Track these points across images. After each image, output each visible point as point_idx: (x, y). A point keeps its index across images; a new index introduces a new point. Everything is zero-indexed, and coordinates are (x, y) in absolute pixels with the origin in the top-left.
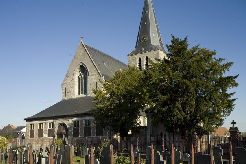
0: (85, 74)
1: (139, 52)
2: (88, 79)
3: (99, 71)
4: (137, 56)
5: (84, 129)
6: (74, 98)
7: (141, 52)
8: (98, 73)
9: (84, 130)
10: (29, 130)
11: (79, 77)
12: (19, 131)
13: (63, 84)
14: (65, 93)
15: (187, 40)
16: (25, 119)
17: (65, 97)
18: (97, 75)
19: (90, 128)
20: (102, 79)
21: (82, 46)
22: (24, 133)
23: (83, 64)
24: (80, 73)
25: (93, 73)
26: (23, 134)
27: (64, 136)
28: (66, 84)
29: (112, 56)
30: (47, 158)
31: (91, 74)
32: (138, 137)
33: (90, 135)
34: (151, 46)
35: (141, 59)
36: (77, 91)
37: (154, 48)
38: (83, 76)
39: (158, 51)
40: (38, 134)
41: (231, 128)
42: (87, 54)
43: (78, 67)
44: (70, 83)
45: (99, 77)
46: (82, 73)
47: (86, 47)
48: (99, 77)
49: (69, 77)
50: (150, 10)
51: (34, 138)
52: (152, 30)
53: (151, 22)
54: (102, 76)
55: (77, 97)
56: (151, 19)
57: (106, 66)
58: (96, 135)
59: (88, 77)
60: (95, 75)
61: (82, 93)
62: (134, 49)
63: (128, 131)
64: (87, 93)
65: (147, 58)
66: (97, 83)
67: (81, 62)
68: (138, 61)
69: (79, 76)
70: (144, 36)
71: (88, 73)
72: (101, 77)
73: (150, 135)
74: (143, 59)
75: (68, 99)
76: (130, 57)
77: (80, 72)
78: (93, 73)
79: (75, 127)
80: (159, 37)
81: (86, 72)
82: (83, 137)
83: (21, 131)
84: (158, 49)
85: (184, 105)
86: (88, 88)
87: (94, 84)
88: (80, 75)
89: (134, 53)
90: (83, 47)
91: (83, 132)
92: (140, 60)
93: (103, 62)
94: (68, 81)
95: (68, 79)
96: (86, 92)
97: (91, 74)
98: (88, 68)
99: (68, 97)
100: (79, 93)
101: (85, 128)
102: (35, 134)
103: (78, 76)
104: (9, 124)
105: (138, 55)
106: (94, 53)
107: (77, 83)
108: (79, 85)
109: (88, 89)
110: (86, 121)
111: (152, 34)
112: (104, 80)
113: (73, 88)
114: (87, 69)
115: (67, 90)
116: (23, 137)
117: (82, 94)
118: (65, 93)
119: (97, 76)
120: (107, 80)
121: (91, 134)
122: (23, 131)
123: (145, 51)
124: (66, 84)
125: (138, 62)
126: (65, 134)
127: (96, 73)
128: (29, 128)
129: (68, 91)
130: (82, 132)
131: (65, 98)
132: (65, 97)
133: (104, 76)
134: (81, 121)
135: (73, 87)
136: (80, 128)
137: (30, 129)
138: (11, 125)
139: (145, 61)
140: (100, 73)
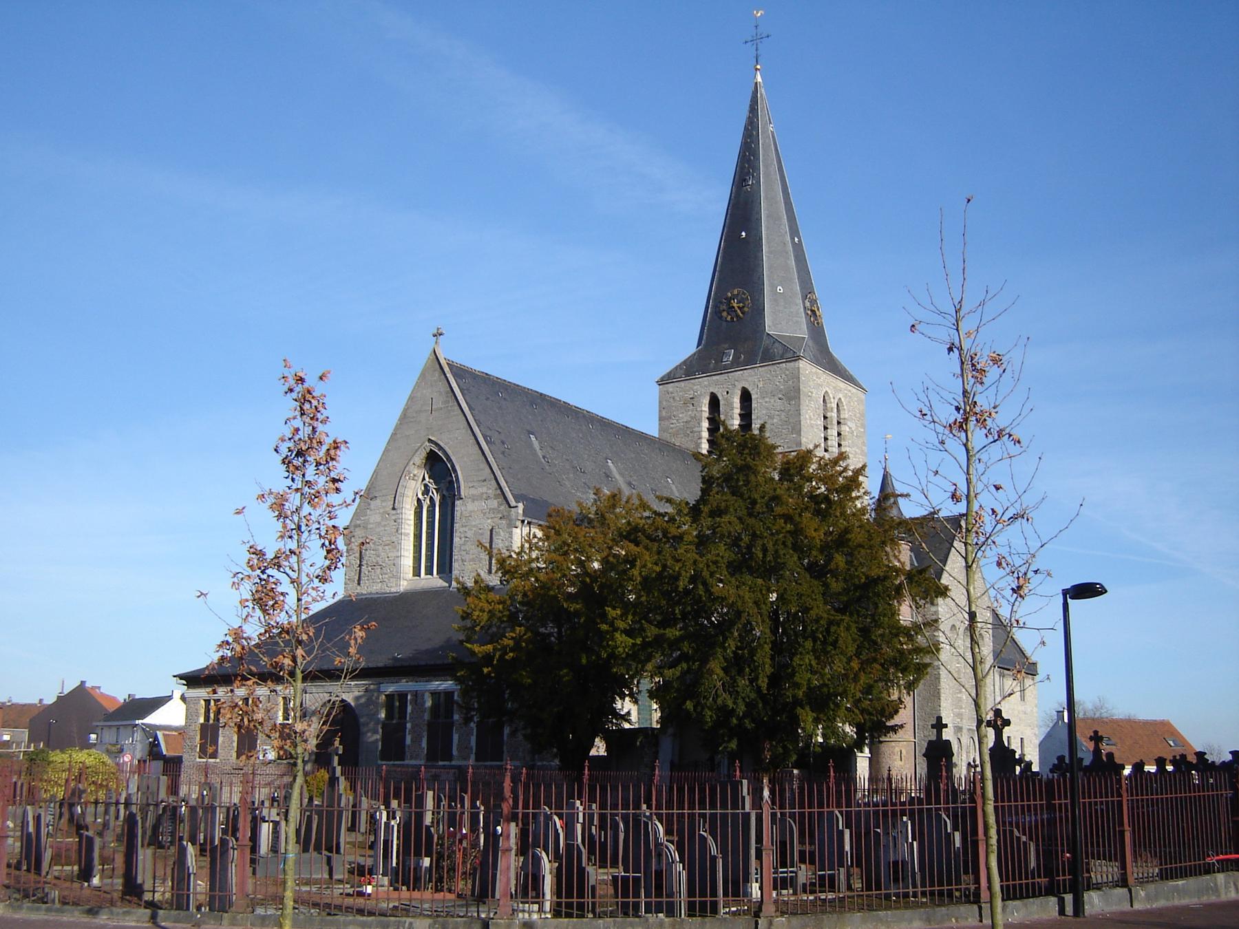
0: (447, 490)
1: (712, 365)
2: (457, 514)
3: (503, 484)
4: (703, 387)
5: (425, 728)
6: (393, 590)
7: (720, 369)
8: (499, 492)
9: (425, 734)
10: (198, 728)
11: (419, 500)
12: (137, 722)
13: (352, 529)
14: (360, 566)
15: (767, 435)
16: (181, 677)
17: (359, 584)
18: (496, 497)
19: (452, 724)
20: (513, 517)
21: (438, 373)
22: (160, 734)
23: (440, 448)
24: (426, 486)
25: (480, 490)
26: (156, 738)
27: (336, 758)
28: (365, 528)
29: (574, 400)
30: (276, 824)
31: (473, 491)
32: (586, 772)
33: (449, 757)
34: (766, 341)
35: (720, 398)
36: (408, 561)
37: (777, 349)
38: (437, 498)
39: (796, 364)
40: (235, 744)
41: (930, 743)
42: (457, 407)
43: (419, 458)
44: (379, 523)
45: (504, 507)
46: (432, 486)
47: (455, 375)
48: (502, 508)
49: (378, 502)
50: (767, 175)
51: (218, 760)
52: (770, 268)
53: (767, 228)
54: (513, 503)
55: (409, 588)
56: (768, 216)
57: (540, 454)
58: (473, 757)
59: (457, 503)
60: (488, 498)
61: (429, 571)
62: (686, 345)
63: (591, 745)
64: (451, 571)
65: (746, 397)
66: (491, 531)
67: (430, 440)
68: (706, 408)
69: (420, 496)
70: (736, 292)
71: (459, 487)
72: (510, 507)
73: (672, 763)
74: (726, 400)
75: (371, 594)
76: (670, 387)
77: (424, 479)
78: (480, 490)
79: (392, 719)
80: (804, 298)
81: (451, 482)
82: (422, 762)
83: (146, 720)
84: (797, 358)
85: (737, 665)
86: (455, 552)
87: (482, 534)
88: (426, 491)
89: (691, 369)
90: (443, 376)
91: (424, 744)
92: (714, 402)
93: (530, 433)
94: (374, 518)
95: (372, 507)
96: (445, 569)
97: (473, 491)
98: (458, 468)
99: (372, 587)
100: (417, 572)
101: (429, 725)
102: (223, 742)
103: (415, 498)
104: (83, 683)
105: (705, 381)
106: (487, 399)
107: (409, 528)
108: (418, 537)
109: (455, 557)
110: (434, 694)
111: (195, 881)
112: (523, 522)
113: (395, 547)
114: (455, 471)
115: (369, 556)
116: (155, 749)
117: (432, 574)
118: (360, 566)
119: (494, 503)
120: (534, 521)
121: (455, 752)
122: (154, 719)
123: (737, 364)
124: (365, 528)
125: (706, 414)
126: (340, 752)
127: (490, 489)
128: (198, 716)
129: (374, 559)
130: (417, 740)
131: (359, 590)
132: (359, 584)
133: (521, 506)
134: (416, 694)
135: (395, 545)
136: (409, 725)
137: (202, 720)
138: (93, 688)
139: (737, 411)
140: (506, 490)
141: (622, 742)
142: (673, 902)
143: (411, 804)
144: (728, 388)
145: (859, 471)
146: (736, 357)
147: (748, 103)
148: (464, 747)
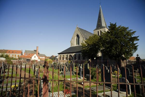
4: (97, 31)
7: (99, 29)
36: (75, 44)
43: (76, 35)
62: (96, 28)
65: (101, 31)
88: (77, 38)
89: (96, 29)
92: (98, 32)
96: (79, 44)
99: (73, 46)
100: (76, 45)
108: (76, 42)
122: (57, 57)
123: (100, 29)
141: (98, 58)
142: (125, 85)
143: (134, 92)
144: (99, 31)
145: (30, 96)
146: (100, 28)
147: (99, 11)
148: (81, 58)
